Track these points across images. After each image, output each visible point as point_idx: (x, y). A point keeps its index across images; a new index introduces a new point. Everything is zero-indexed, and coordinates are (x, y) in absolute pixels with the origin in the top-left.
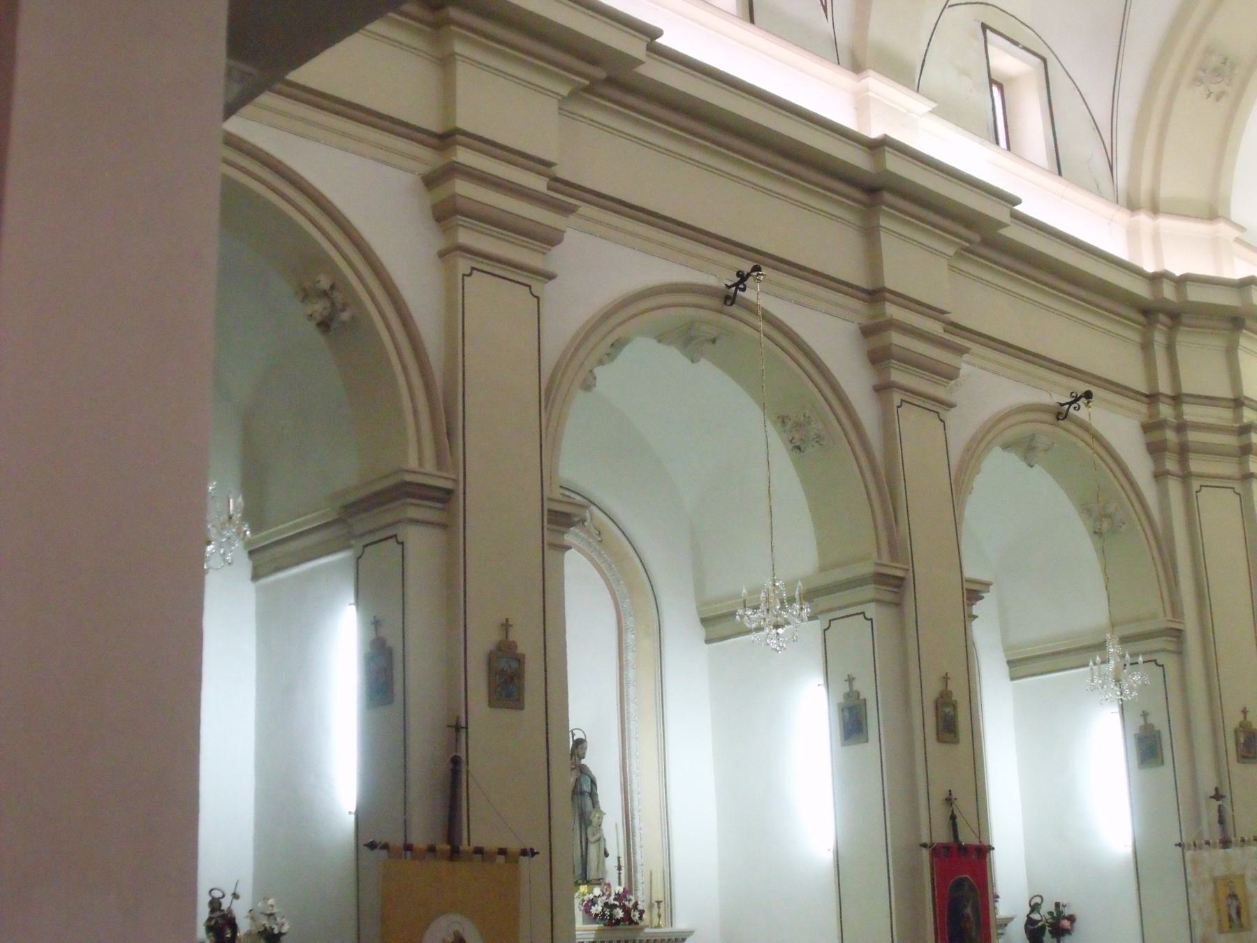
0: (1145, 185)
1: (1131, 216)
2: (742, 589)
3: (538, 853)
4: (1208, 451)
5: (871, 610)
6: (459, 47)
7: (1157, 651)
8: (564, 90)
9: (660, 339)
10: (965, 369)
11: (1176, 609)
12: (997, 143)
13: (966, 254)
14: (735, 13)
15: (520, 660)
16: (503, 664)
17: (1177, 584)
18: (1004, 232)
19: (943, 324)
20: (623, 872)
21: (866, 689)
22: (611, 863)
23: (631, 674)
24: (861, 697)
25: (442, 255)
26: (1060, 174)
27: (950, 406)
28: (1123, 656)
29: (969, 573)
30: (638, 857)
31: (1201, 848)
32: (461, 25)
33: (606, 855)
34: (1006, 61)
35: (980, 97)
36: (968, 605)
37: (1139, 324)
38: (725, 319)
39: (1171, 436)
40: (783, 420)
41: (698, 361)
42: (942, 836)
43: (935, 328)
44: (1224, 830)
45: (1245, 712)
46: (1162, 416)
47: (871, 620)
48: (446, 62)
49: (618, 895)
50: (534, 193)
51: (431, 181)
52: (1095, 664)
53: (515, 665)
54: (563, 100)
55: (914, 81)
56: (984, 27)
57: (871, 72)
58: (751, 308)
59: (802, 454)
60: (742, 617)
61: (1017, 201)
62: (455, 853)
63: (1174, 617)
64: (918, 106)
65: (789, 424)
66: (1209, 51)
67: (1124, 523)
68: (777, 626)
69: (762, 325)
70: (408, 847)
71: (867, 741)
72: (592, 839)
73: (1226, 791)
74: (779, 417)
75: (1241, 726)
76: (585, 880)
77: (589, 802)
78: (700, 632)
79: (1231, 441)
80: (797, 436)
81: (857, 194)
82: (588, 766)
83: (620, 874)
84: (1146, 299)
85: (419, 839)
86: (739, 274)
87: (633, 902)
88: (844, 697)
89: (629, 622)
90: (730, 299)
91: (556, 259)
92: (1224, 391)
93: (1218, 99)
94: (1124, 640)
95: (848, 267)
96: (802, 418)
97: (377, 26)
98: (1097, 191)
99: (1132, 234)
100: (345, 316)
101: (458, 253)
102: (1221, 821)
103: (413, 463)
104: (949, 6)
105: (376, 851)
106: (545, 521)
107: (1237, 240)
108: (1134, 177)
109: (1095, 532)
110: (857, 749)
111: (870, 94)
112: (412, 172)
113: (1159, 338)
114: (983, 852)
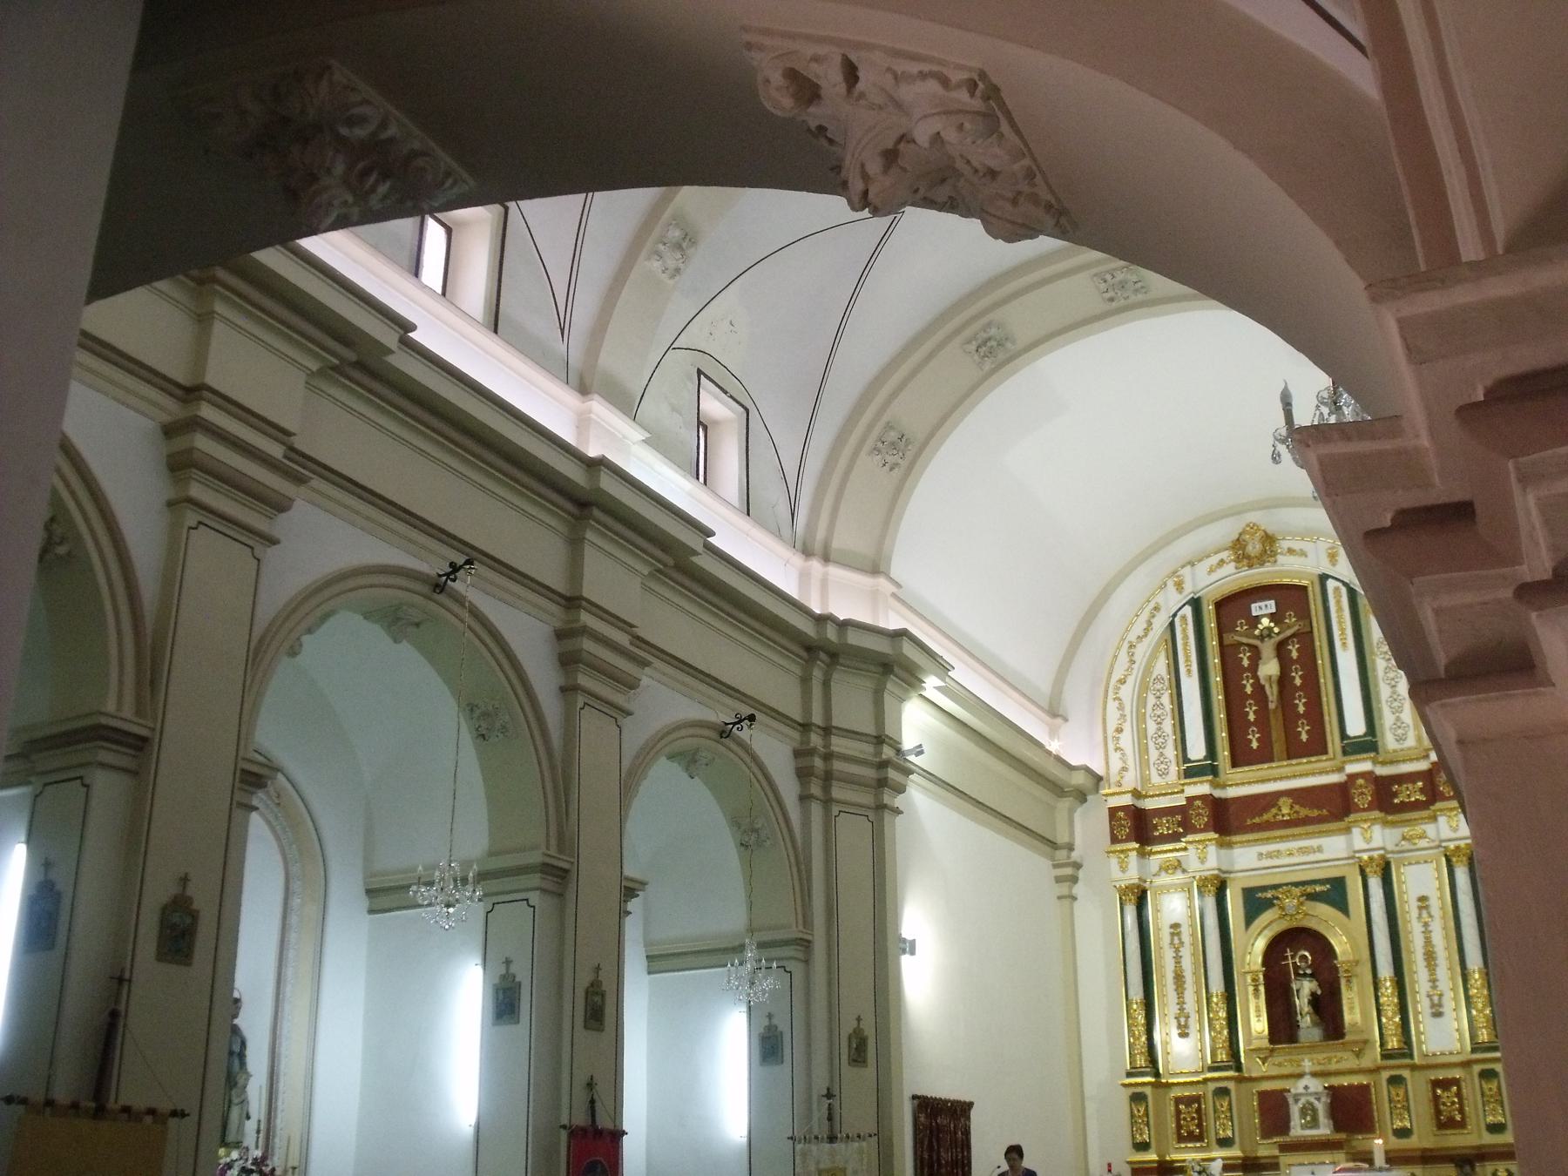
0: (820, 534)
1: (806, 560)
2: (418, 867)
3: (188, 1115)
4: (851, 781)
5: (535, 898)
6: (220, 307)
7: (788, 958)
8: (314, 366)
9: (367, 616)
10: (645, 681)
11: (807, 922)
12: (698, 479)
13: (658, 575)
14: (480, 320)
15: (194, 916)
16: (176, 918)
17: (810, 896)
18: (695, 559)
19: (630, 637)
20: (261, 1135)
21: (522, 973)
22: (250, 1126)
23: (292, 937)
24: (517, 980)
25: (171, 504)
26: (748, 514)
27: (629, 713)
28: (761, 961)
29: (628, 872)
30: (278, 1121)
31: (810, 1142)
32: (598, 522)
33: (248, 1118)
34: (714, 406)
35: (689, 435)
36: (624, 901)
37: (801, 658)
38: (432, 606)
39: (818, 763)
40: (472, 708)
41: (400, 642)
42: (581, 1119)
43: (622, 639)
44: (832, 1127)
45: (859, 1019)
46: (812, 745)
47: (534, 907)
48: (204, 319)
49: (256, 1159)
50: (257, 451)
51: (169, 431)
52: (732, 965)
53: (188, 921)
54: (312, 374)
55: (633, 409)
56: (699, 372)
57: (596, 396)
58: (459, 600)
59: (485, 742)
60: (415, 892)
61: (711, 533)
62: (100, 1112)
63: (804, 928)
64: (635, 434)
65: (478, 712)
66: (889, 426)
67: (768, 838)
68: (448, 906)
69: (466, 616)
70: (49, 1103)
71: (518, 1022)
72: (236, 1100)
73: (836, 1091)
74: (468, 705)
75: (855, 1031)
76: (224, 1143)
77: (236, 1062)
78: (364, 903)
79: (869, 773)
80: (484, 725)
81: (569, 506)
82: (240, 1026)
83: (258, 1138)
84: (811, 637)
85: (62, 1095)
86: (452, 565)
87: (270, 1168)
88: (500, 978)
89: (296, 886)
90: (439, 587)
91: (280, 526)
92: (869, 729)
93: (891, 469)
94: (762, 945)
95: (551, 571)
96: (491, 708)
97: (162, 285)
98: (777, 534)
99: (804, 577)
100: (62, 550)
101: (185, 504)
102: (830, 1118)
103: (111, 707)
104: (674, 349)
105: (13, 1106)
106: (237, 780)
107: (894, 595)
108: (811, 526)
109: (742, 844)
110: (508, 1029)
111: (593, 416)
112: (152, 419)
113: (817, 674)
114: (617, 1135)
